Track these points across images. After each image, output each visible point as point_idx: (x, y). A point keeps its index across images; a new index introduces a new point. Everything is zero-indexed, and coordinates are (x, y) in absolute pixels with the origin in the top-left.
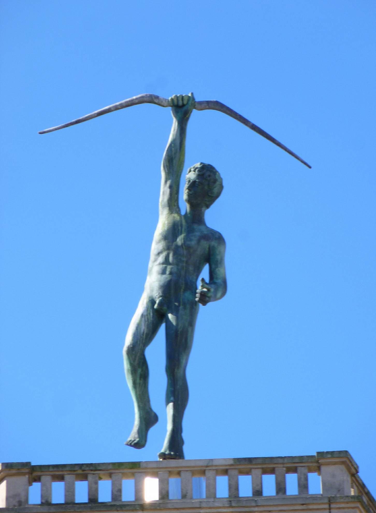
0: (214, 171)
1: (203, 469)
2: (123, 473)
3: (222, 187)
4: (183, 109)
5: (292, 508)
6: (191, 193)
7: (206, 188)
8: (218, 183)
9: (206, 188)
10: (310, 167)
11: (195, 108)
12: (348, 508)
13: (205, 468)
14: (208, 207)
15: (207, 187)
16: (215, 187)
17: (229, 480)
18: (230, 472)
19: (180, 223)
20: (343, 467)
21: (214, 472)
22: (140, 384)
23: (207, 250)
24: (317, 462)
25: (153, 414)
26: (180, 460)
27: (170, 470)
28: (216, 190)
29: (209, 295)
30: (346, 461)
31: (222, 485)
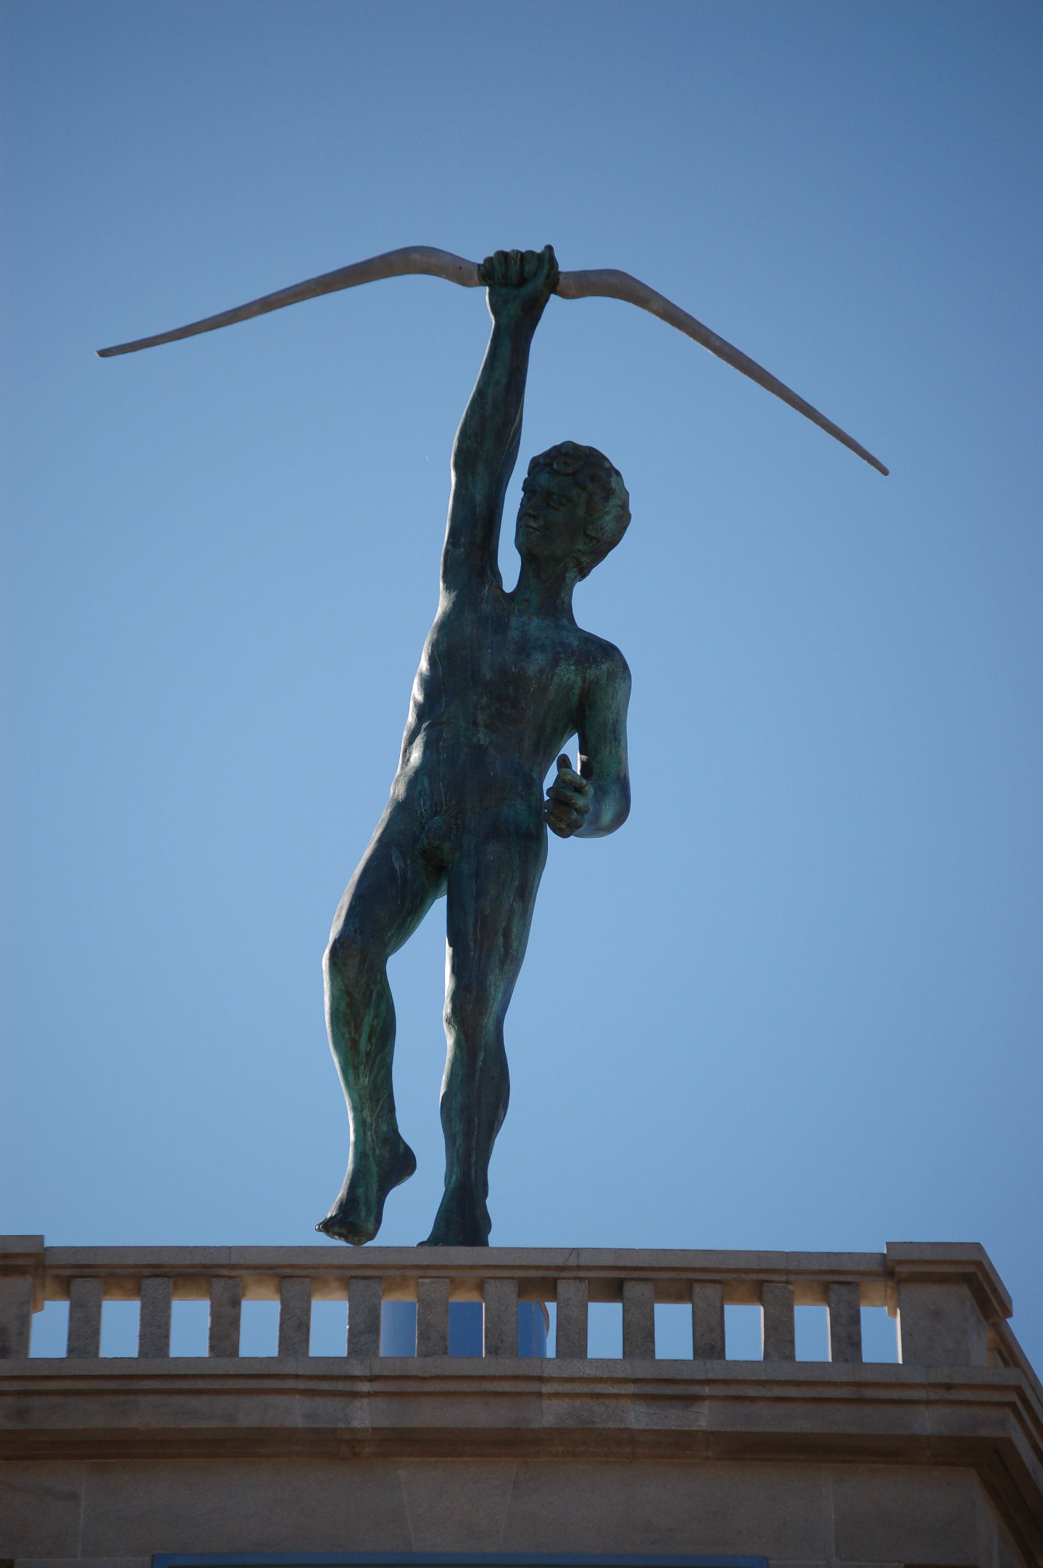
0: (607, 465)
1: (543, 1277)
2: (452, 1280)
3: (624, 519)
4: (521, 286)
5: (810, 1392)
6: (542, 461)
7: (581, 512)
8: (615, 501)
9: (581, 512)
10: (885, 472)
11: (556, 293)
12: (982, 1404)
13: (623, 1275)
14: (583, 572)
15: (580, 504)
16: (607, 513)
17: (625, 1311)
18: (629, 1289)
19: (547, 256)
20: (964, 1290)
21: (584, 1286)
22: (368, 1054)
23: (575, 699)
24: (902, 1271)
25: (402, 1149)
26: (477, 1249)
27: (452, 1273)
28: (608, 522)
29: (580, 802)
30: (975, 1274)
31: (605, 1327)
